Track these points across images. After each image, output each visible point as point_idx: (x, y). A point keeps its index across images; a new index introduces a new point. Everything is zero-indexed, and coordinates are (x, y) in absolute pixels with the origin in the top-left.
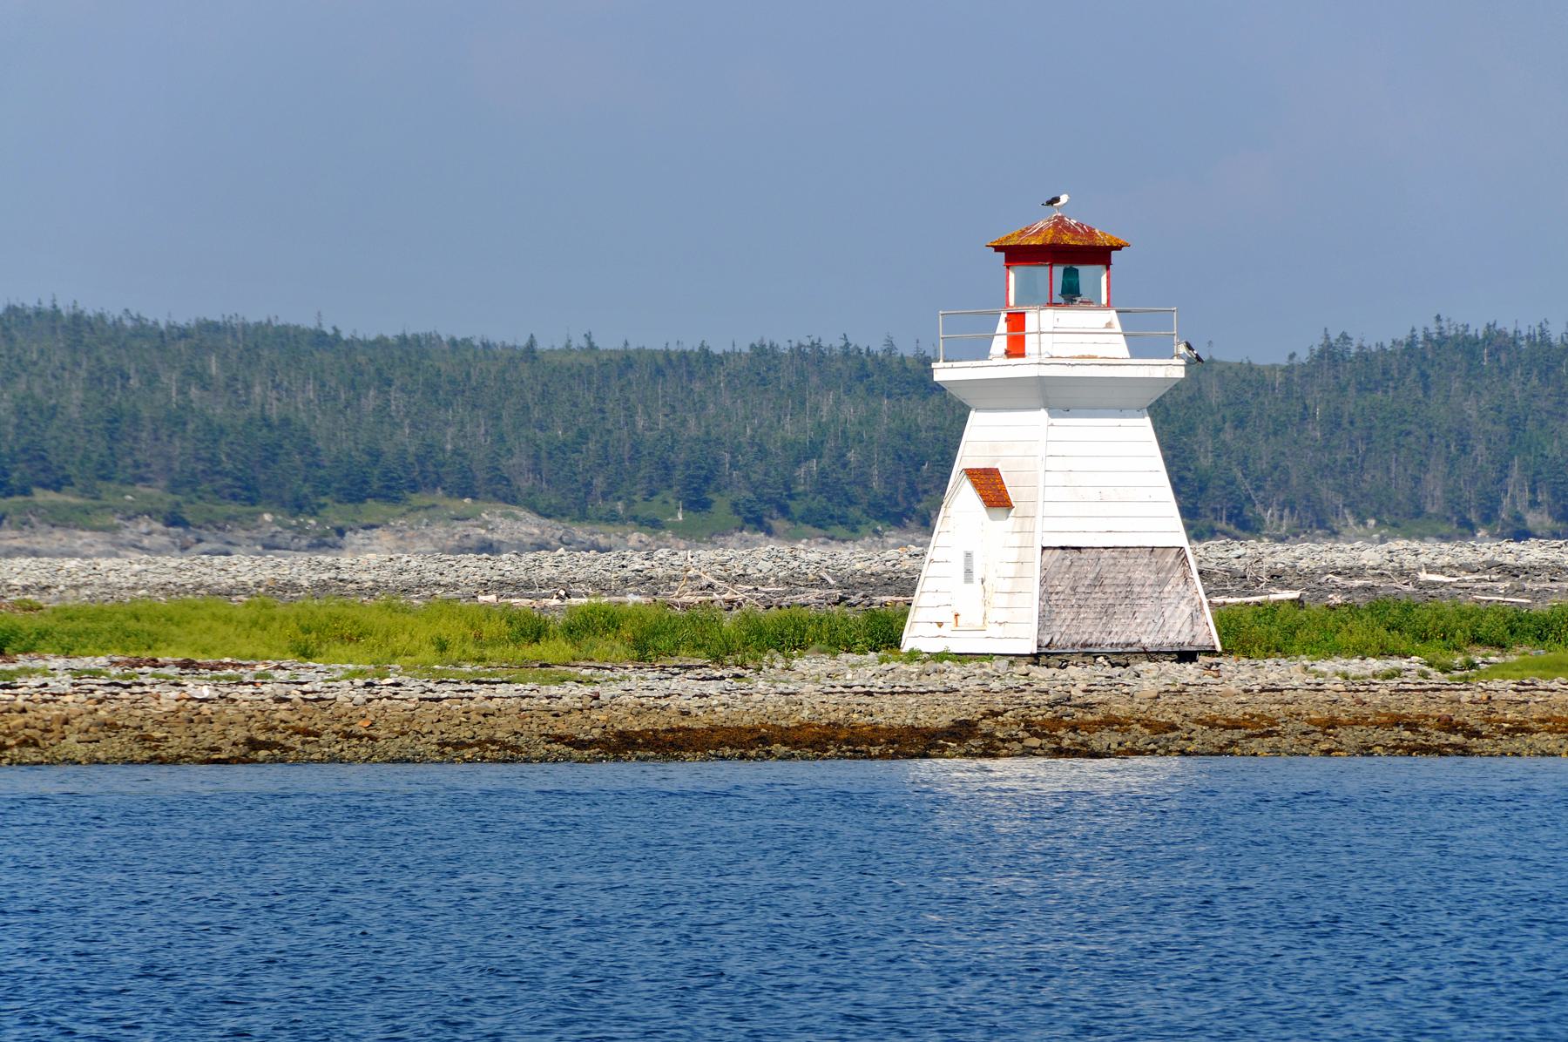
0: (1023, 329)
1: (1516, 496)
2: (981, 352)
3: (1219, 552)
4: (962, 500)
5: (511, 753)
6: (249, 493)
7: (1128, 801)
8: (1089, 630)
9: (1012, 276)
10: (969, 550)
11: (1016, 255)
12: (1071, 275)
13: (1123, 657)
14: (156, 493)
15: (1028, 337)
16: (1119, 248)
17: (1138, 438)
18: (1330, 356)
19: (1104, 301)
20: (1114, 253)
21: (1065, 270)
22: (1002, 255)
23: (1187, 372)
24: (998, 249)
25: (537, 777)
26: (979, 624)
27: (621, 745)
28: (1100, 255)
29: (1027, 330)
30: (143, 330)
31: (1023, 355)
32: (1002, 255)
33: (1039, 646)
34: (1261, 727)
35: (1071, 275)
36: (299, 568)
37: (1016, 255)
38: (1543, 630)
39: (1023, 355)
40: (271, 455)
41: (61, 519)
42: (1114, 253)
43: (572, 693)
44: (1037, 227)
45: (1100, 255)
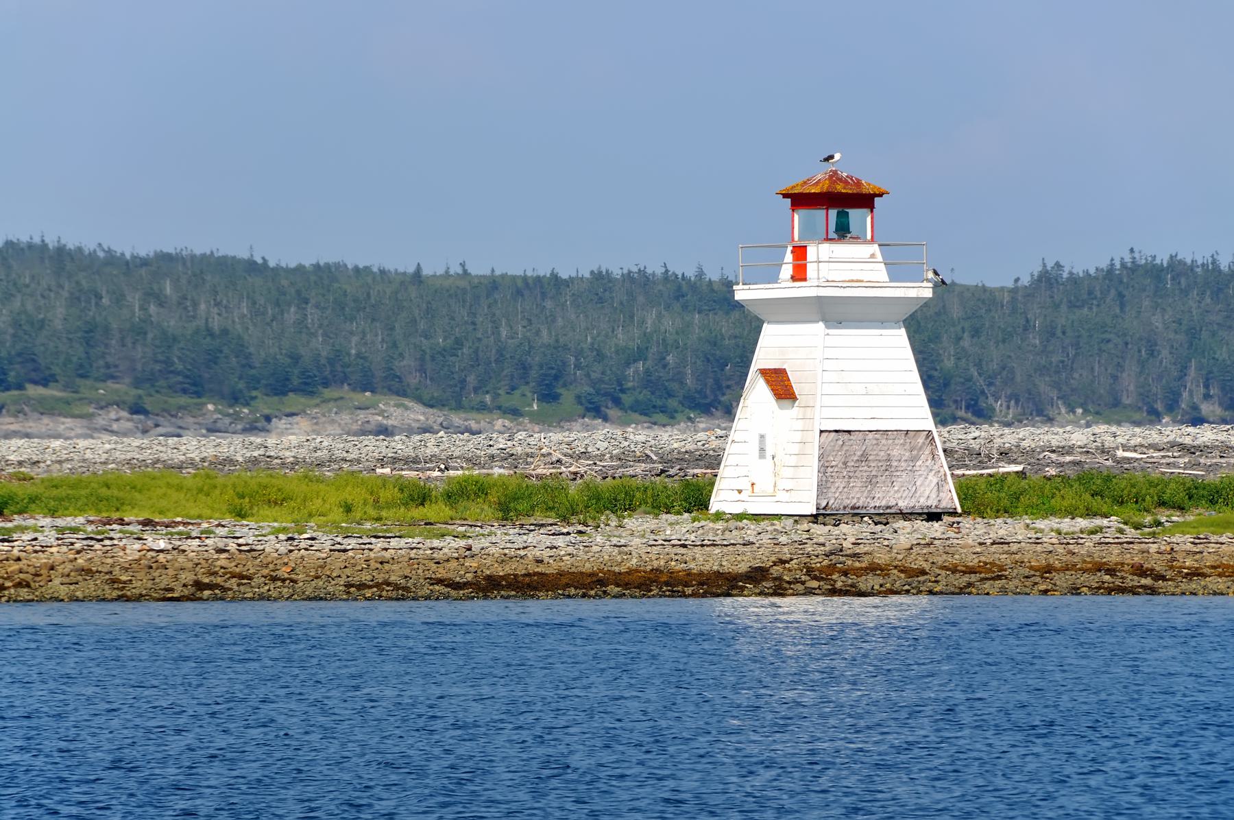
0: (806, 259)
1: (1193, 391)
2: (773, 278)
3: (960, 435)
4: (757, 394)
5: (402, 592)
6: (196, 387)
7: (888, 631)
8: (857, 496)
9: (796, 217)
10: (762, 433)
11: (800, 200)
12: (843, 216)
13: (884, 517)
14: (123, 387)
15: (808, 264)
16: (880, 195)
17: (896, 344)
18: (1047, 279)
19: (869, 237)
20: (876, 199)
21: (838, 213)
22: (789, 201)
23: (934, 293)
24: (785, 196)
25: (423, 612)
26: (770, 491)
27: (489, 586)
28: (866, 201)
29: (808, 260)
30: (112, 260)
31: (805, 279)
32: (789, 201)
33: (818, 509)
34: (993, 572)
35: (843, 216)
36: (235, 447)
37: (800, 200)
38: (1214, 496)
39: (805, 279)
40: (213, 358)
41: (48, 409)
42: (876, 199)
43: (450, 546)
44: (815, 177)
45: (866, 201)
